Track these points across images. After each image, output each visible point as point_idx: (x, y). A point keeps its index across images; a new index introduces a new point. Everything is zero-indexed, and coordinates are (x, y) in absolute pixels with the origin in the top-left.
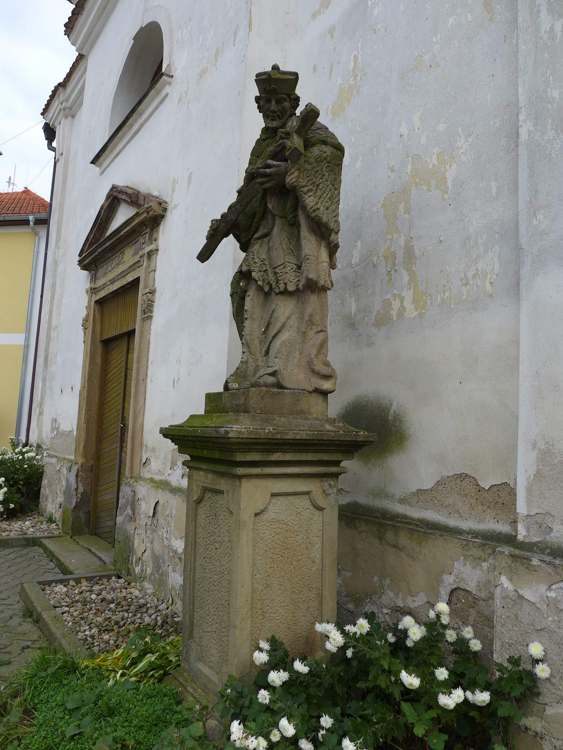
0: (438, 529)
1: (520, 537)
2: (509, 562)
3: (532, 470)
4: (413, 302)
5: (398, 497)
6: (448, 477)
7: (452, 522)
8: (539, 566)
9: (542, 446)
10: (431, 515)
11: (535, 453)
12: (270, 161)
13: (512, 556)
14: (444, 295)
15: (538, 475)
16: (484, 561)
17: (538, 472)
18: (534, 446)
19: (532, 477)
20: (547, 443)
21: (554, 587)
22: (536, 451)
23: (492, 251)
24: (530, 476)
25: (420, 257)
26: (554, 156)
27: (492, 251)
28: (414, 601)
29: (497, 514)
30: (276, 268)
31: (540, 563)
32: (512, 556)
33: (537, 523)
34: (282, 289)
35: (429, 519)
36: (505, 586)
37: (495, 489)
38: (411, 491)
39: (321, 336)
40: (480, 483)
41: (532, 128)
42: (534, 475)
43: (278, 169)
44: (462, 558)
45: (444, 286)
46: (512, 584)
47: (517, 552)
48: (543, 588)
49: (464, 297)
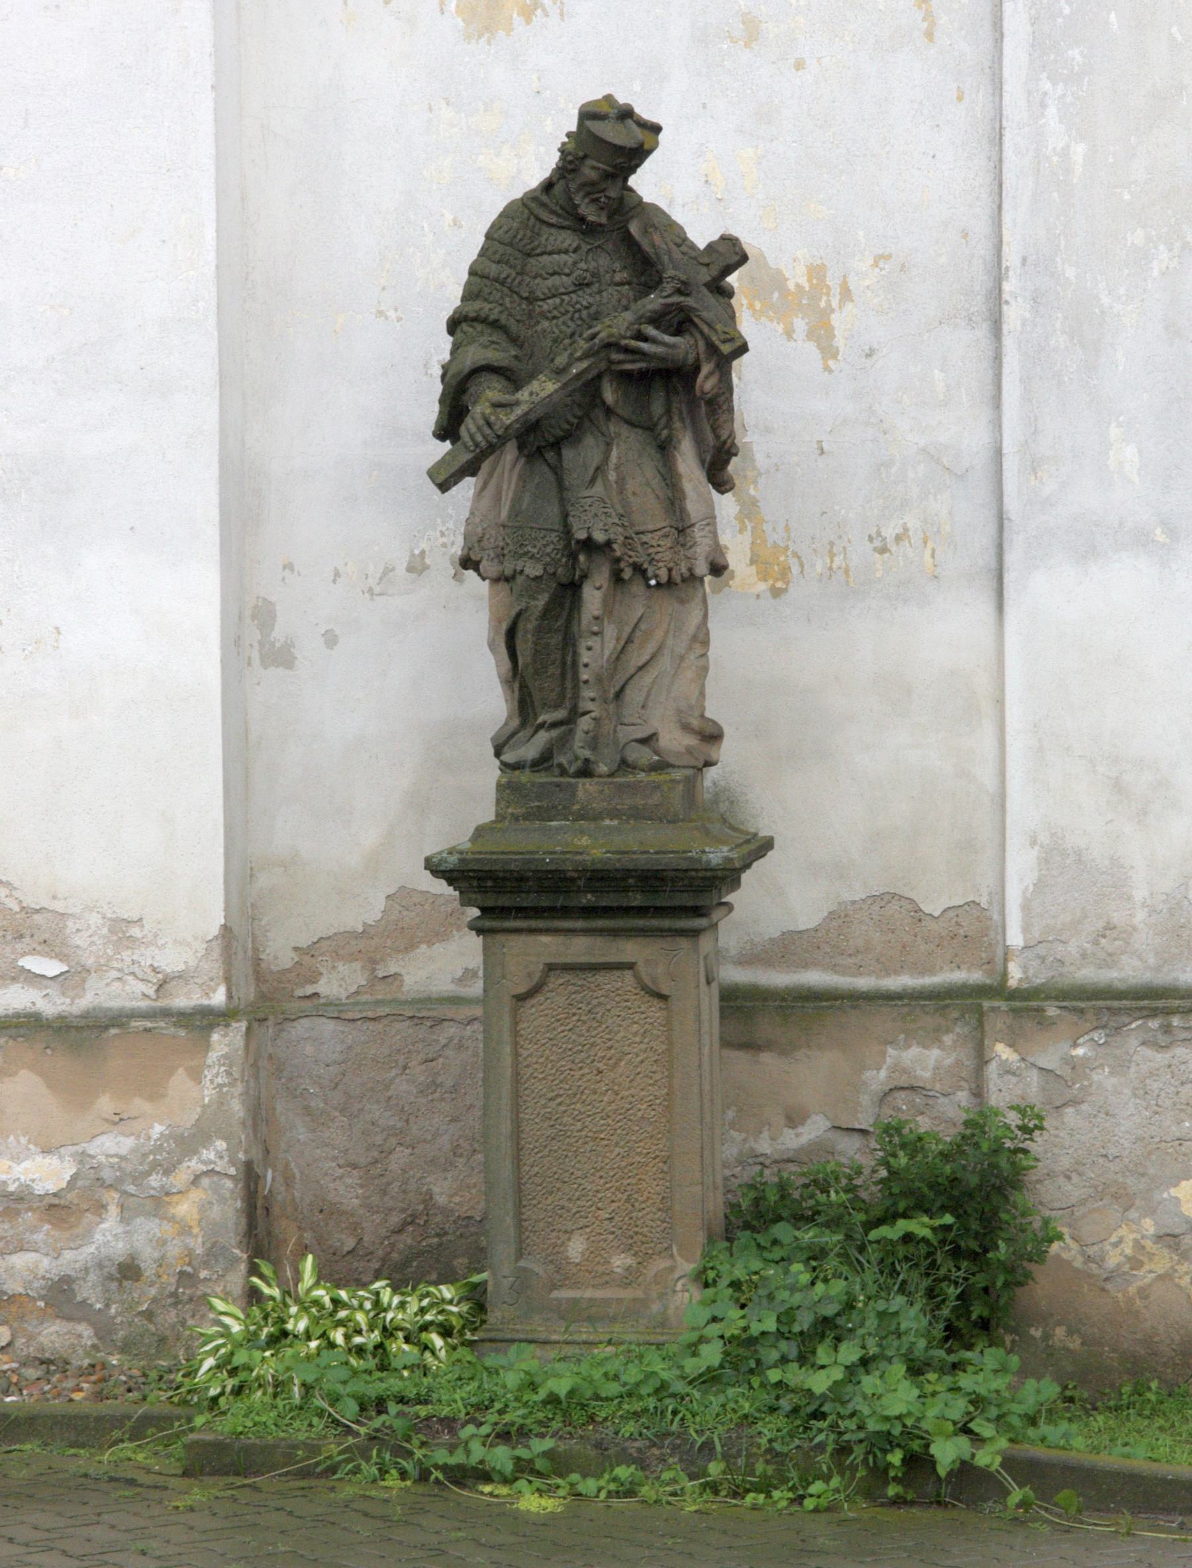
0: (836, 999)
1: (1013, 983)
2: (1008, 1022)
3: (1031, 878)
4: (753, 562)
5: (733, 952)
6: (854, 902)
7: (864, 983)
8: (1059, 1016)
9: (1044, 838)
10: (815, 978)
11: (1034, 853)
12: (651, 331)
13: (1013, 1010)
14: (832, 562)
15: (1040, 886)
16: (948, 1031)
17: (1039, 880)
18: (1033, 843)
19: (1031, 888)
20: (1052, 835)
21: (1081, 1040)
22: (1037, 848)
23: (935, 499)
24: (1027, 888)
25: (768, 472)
26: (1066, 379)
27: (935, 499)
28: (797, 1135)
29: (956, 955)
30: (642, 533)
31: (1058, 1012)
32: (1013, 1010)
33: (1038, 956)
34: (664, 578)
35: (812, 983)
36: (1004, 1057)
37: (951, 914)
38: (767, 937)
39: (702, 662)
40: (922, 906)
41: (1028, 315)
42: (1034, 885)
43: (670, 351)
44: (902, 1036)
45: (832, 544)
46: (1016, 1051)
47: (1018, 1004)
48: (1064, 1046)
49: (878, 575)
